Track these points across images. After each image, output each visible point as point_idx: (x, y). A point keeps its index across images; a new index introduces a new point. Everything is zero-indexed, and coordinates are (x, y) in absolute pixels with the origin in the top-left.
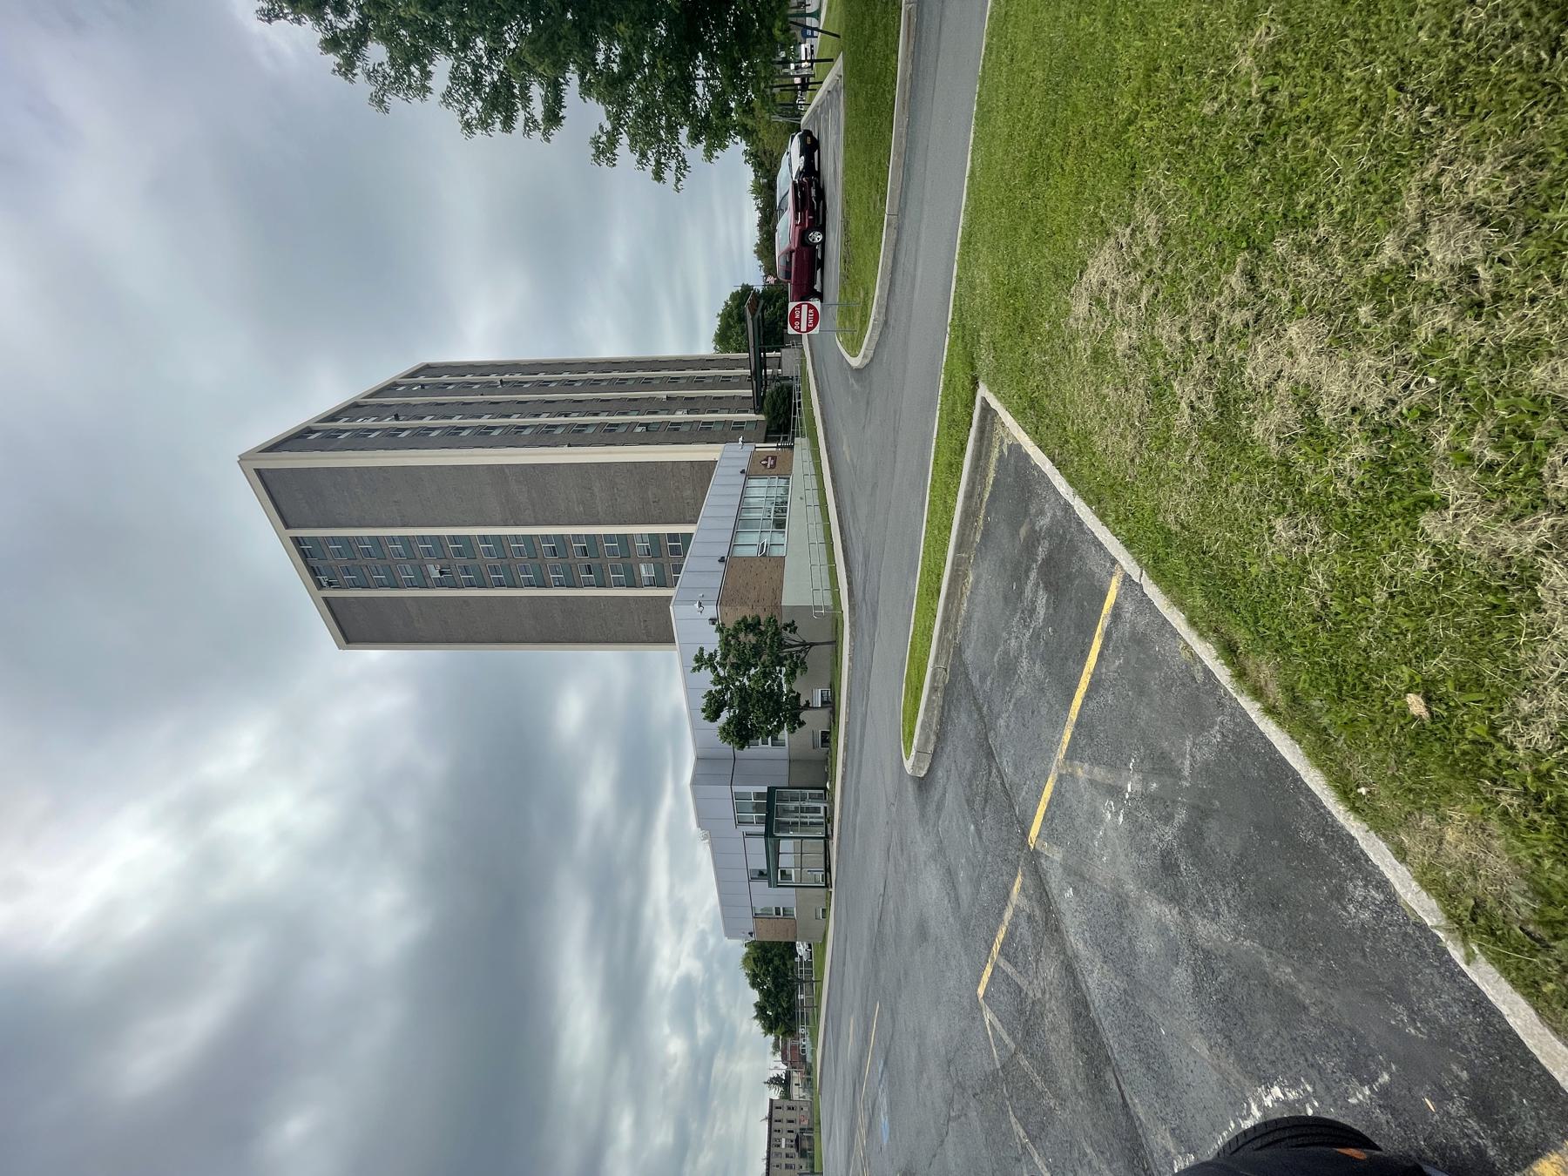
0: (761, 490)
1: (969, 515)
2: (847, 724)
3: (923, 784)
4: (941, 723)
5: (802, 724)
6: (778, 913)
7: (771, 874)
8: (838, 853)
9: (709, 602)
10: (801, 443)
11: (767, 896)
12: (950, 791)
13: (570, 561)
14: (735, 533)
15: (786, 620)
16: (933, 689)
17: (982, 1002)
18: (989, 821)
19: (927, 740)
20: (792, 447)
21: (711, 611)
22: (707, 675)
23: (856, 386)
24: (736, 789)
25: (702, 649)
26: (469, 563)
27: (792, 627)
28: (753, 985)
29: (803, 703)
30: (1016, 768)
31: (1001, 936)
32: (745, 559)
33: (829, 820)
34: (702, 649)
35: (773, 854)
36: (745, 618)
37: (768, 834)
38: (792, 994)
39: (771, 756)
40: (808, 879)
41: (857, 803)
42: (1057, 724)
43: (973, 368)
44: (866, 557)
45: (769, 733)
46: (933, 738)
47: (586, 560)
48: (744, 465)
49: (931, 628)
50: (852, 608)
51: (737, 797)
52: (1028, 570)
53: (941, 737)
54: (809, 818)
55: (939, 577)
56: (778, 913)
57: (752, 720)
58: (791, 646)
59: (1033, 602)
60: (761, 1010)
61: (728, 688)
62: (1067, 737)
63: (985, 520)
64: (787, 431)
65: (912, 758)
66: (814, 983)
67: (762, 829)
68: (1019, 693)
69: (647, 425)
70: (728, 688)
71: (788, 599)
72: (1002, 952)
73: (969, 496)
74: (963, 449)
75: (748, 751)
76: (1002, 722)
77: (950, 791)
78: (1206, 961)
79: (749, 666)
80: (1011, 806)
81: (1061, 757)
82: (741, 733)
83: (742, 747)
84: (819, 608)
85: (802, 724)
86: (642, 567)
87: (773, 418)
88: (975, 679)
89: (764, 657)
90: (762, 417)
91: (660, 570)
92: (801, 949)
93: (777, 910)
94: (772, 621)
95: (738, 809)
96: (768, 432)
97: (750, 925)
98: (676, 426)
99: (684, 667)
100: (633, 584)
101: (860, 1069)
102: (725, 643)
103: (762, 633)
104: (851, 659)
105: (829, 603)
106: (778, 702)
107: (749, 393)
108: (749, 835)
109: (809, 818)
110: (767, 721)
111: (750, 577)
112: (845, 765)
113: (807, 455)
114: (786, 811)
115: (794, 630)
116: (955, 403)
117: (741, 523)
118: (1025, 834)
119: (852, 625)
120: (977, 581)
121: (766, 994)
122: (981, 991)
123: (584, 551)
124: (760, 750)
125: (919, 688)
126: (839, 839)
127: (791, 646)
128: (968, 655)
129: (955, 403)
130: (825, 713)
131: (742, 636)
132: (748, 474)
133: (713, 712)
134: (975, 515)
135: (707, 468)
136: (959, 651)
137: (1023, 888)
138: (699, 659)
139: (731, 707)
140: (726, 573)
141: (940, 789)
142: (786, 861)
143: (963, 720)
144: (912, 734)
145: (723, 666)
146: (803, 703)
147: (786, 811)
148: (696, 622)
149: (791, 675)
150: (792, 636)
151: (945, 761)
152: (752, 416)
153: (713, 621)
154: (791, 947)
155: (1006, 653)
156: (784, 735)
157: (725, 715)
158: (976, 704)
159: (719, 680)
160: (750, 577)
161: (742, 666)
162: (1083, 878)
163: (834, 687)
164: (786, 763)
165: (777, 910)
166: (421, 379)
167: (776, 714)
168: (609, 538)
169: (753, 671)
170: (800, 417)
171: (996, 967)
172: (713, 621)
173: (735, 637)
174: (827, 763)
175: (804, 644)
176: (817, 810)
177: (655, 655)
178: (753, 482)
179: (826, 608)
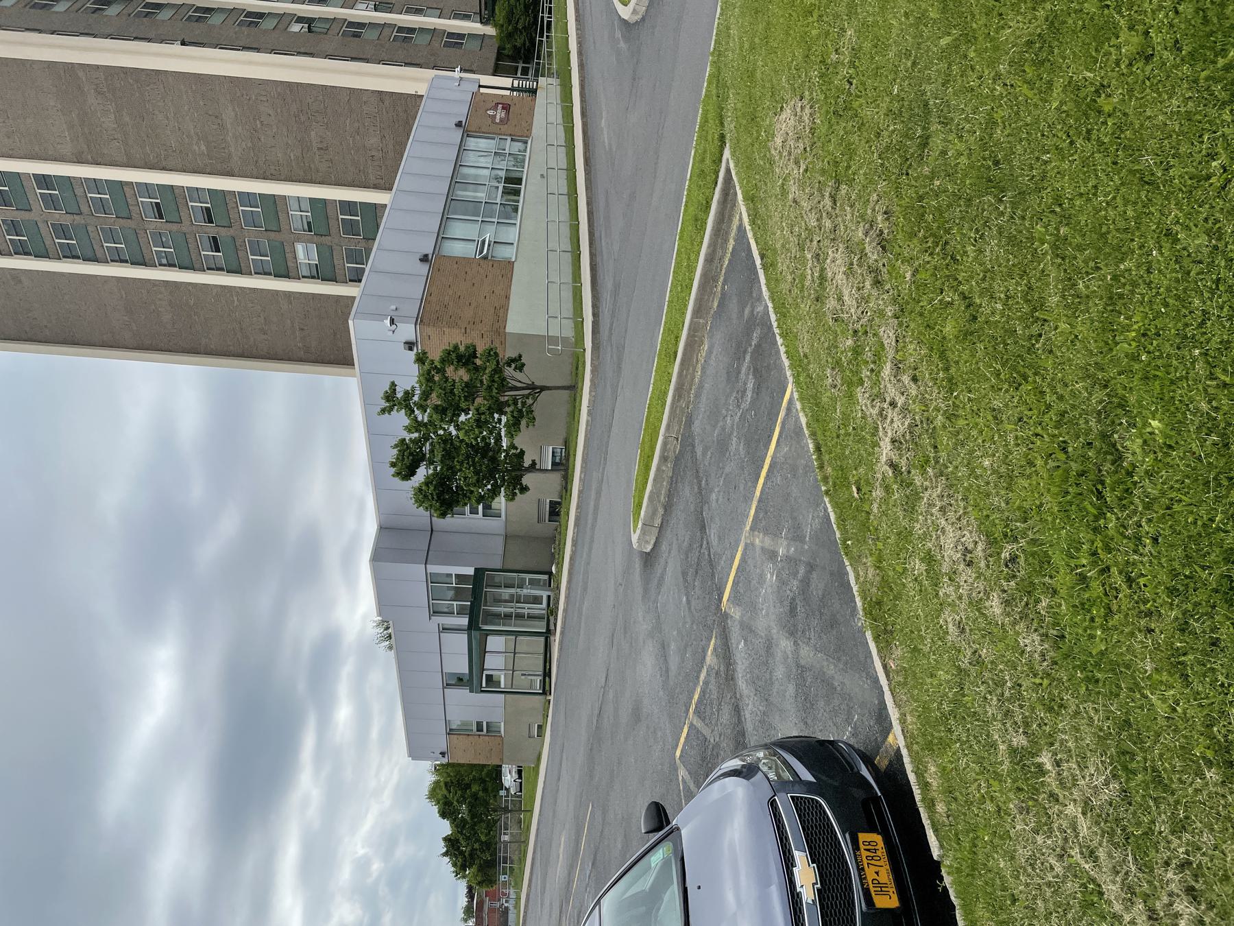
0: (484, 159)
1: (709, 279)
2: (580, 492)
3: (648, 559)
4: (670, 495)
5: (524, 489)
6: (480, 728)
7: (475, 679)
8: (560, 649)
9: (405, 319)
10: (547, 86)
11: (468, 706)
12: (671, 566)
13: (185, 227)
14: (445, 220)
15: (511, 353)
16: (664, 459)
17: (678, 761)
18: (698, 591)
19: (654, 513)
20: (533, 92)
21: (408, 331)
22: (400, 418)
23: (622, 45)
24: (433, 569)
25: (393, 385)
26: (20, 216)
27: (517, 362)
28: (443, 815)
29: (527, 463)
30: (720, 538)
31: (696, 697)
32: (457, 260)
33: (552, 611)
34: (393, 385)
35: (477, 653)
36: (456, 347)
37: (473, 625)
38: (492, 826)
39: (482, 529)
40: (522, 683)
41: (585, 589)
42: (748, 499)
43: (722, 124)
44: (617, 287)
45: (481, 499)
46: (661, 511)
47: (212, 229)
48: (461, 112)
49: (666, 393)
50: (596, 347)
51: (433, 579)
52: (745, 352)
53: (668, 508)
54: (527, 609)
55: (677, 338)
56: (480, 728)
57: (459, 480)
58: (516, 389)
59: (745, 384)
60: (452, 846)
61: (426, 438)
62: (752, 512)
63: (723, 288)
64: (528, 59)
65: (638, 531)
66: (520, 806)
67: (464, 621)
68: (727, 470)
69: (309, 21)
70: (426, 438)
71: (516, 323)
72: (697, 712)
73: (710, 260)
74: (708, 206)
75: (451, 522)
76: (714, 496)
77: (671, 566)
78: (802, 669)
79: (458, 410)
80: (713, 575)
81: (748, 528)
82: (442, 496)
83: (443, 515)
84: (553, 340)
85: (524, 489)
86: (300, 248)
87: (507, 36)
88: (699, 451)
89: (479, 400)
90: (490, 30)
91: (326, 254)
92: (509, 779)
93: (479, 725)
94: (491, 354)
95: (433, 595)
96: (500, 56)
97: (442, 743)
98: (356, 29)
99: (366, 404)
100: (285, 274)
101: (569, 882)
102: (427, 378)
103: (477, 369)
104: (589, 413)
105: (569, 332)
106: (494, 460)
108: (445, 629)
109: (527, 609)
110: (479, 483)
111: (461, 286)
112: (574, 544)
113: (555, 114)
114: (498, 601)
115: (520, 368)
116: (705, 152)
117: (452, 207)
118: (720, 599)
119: (594, 371)
120: (710, 352)
121: (459, 825)
122: (678, 753)
123: (209, 216)
124: (467, 520)
125: (651, 457)
126: (562, 633)
127: (516, 389)
128: (697, 427)
129: (705, 152)
130: (556, 478)
131: (450, 371)
132: (466, 129)
133: (406, 467)
134: (715, 280)
135: (407, 106)
136: (690, 422)
137: (715, 649)
138: (390, 396)
139: (431, 462)
140: (430, 280)
141: (662, 561)
142: (494, 663)
143: (687, 492)
144: (639, 506)
145: (423, 408)
146: (527, 463)
147: (498, 601)
148: (387, 347)
149: (514, 426)
150: (518, 375)
151: (668, 534)
153: (410, 345)
154: (497, 772)
155: (723, 429)
156: (500, 502)
157: (422, 473)
158: (697, 477)
159: (416, 426)
160: (461, 286)
161: (449, 410)
162: (751, 631)
163: (569, 444)
164: (501, 540)
165: (479, 725)
167: (491, 475)
168: (247, 198)
169: (463, 418)
170: (550, 45)
171: (692, 726)
172: (410, 345)
173: (441, 371)
174: (553, 542)
175: (532, 387)
176: (537, 600)
177: (328, 380)
178: (472, 143)
179: (565, 340)
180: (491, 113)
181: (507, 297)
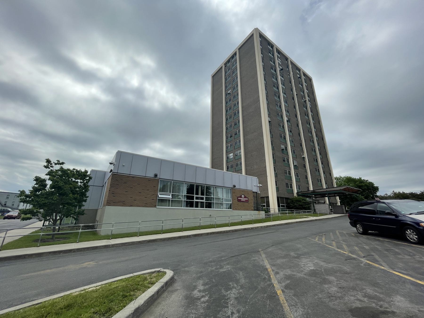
86: (232, 154)
90: (295, 195)
98: (286, 161)
107: (311, 188)
152: (295, 191)
166: (303, 77)
180: (243, 196)
181: (131, 206)
